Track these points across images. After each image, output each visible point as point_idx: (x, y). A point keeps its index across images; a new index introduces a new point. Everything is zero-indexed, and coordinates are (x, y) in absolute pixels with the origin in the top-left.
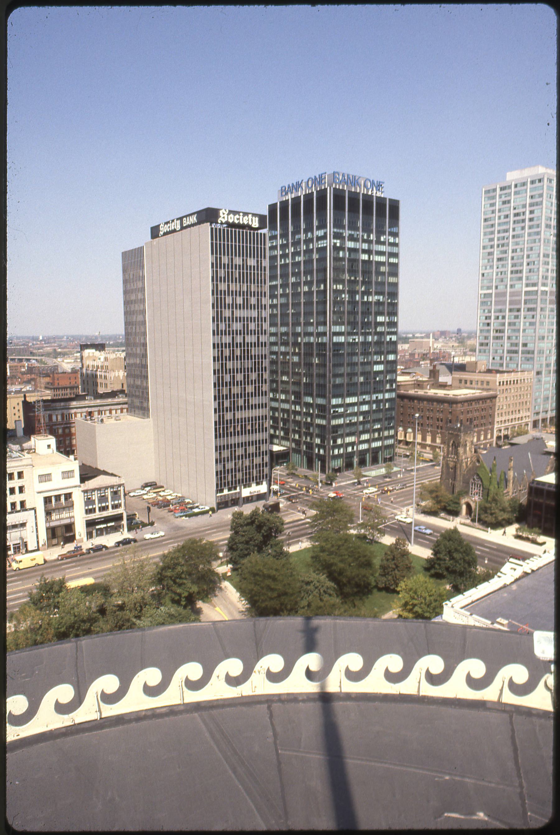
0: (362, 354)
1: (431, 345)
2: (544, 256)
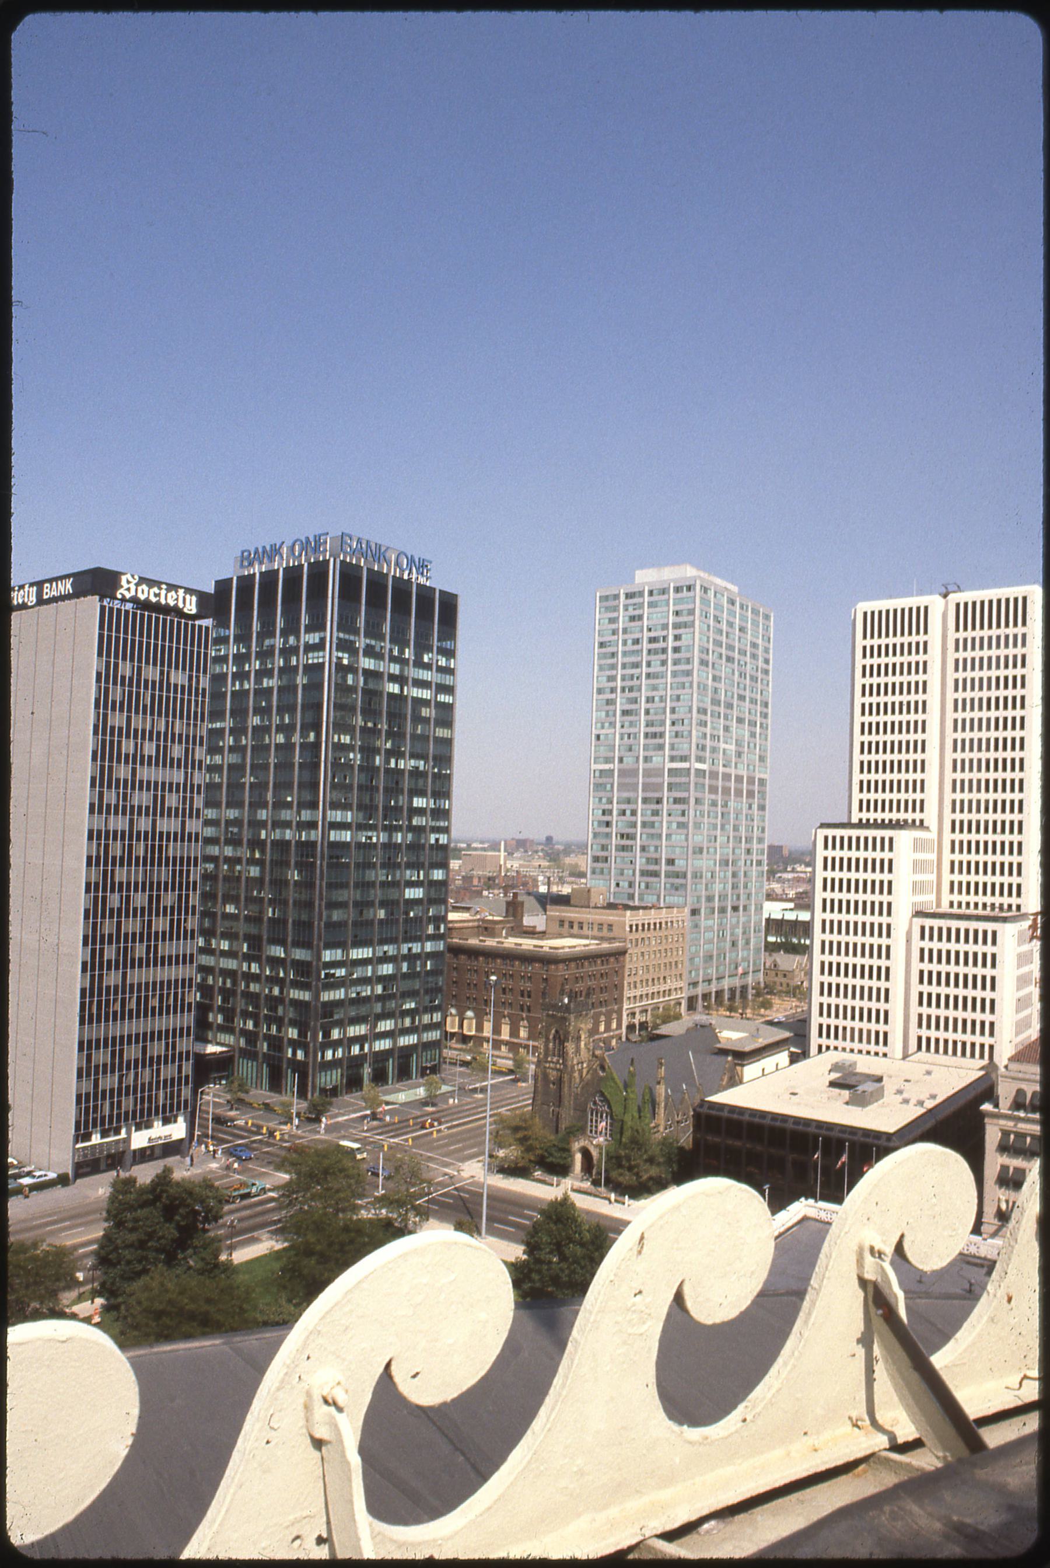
0: (383, 866)
1: (502, 862)
2: (698, 712)
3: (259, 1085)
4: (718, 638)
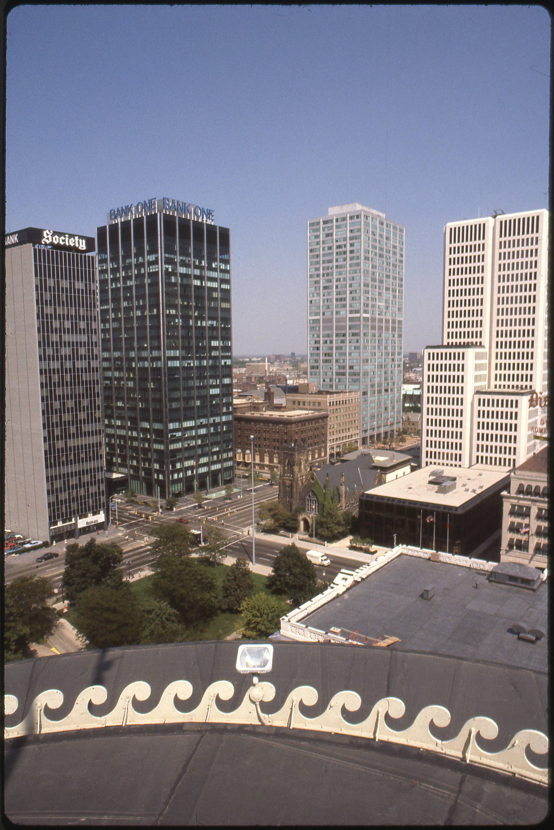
0: (198, 378)
2: (364, 286)
3: (141, 492)
4: (374, 244)
